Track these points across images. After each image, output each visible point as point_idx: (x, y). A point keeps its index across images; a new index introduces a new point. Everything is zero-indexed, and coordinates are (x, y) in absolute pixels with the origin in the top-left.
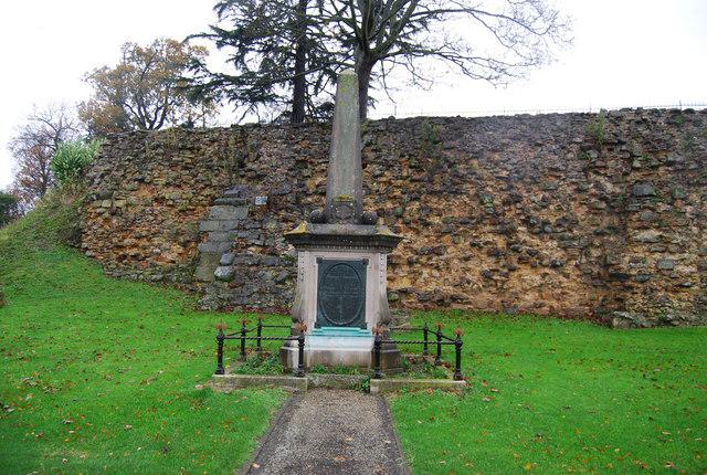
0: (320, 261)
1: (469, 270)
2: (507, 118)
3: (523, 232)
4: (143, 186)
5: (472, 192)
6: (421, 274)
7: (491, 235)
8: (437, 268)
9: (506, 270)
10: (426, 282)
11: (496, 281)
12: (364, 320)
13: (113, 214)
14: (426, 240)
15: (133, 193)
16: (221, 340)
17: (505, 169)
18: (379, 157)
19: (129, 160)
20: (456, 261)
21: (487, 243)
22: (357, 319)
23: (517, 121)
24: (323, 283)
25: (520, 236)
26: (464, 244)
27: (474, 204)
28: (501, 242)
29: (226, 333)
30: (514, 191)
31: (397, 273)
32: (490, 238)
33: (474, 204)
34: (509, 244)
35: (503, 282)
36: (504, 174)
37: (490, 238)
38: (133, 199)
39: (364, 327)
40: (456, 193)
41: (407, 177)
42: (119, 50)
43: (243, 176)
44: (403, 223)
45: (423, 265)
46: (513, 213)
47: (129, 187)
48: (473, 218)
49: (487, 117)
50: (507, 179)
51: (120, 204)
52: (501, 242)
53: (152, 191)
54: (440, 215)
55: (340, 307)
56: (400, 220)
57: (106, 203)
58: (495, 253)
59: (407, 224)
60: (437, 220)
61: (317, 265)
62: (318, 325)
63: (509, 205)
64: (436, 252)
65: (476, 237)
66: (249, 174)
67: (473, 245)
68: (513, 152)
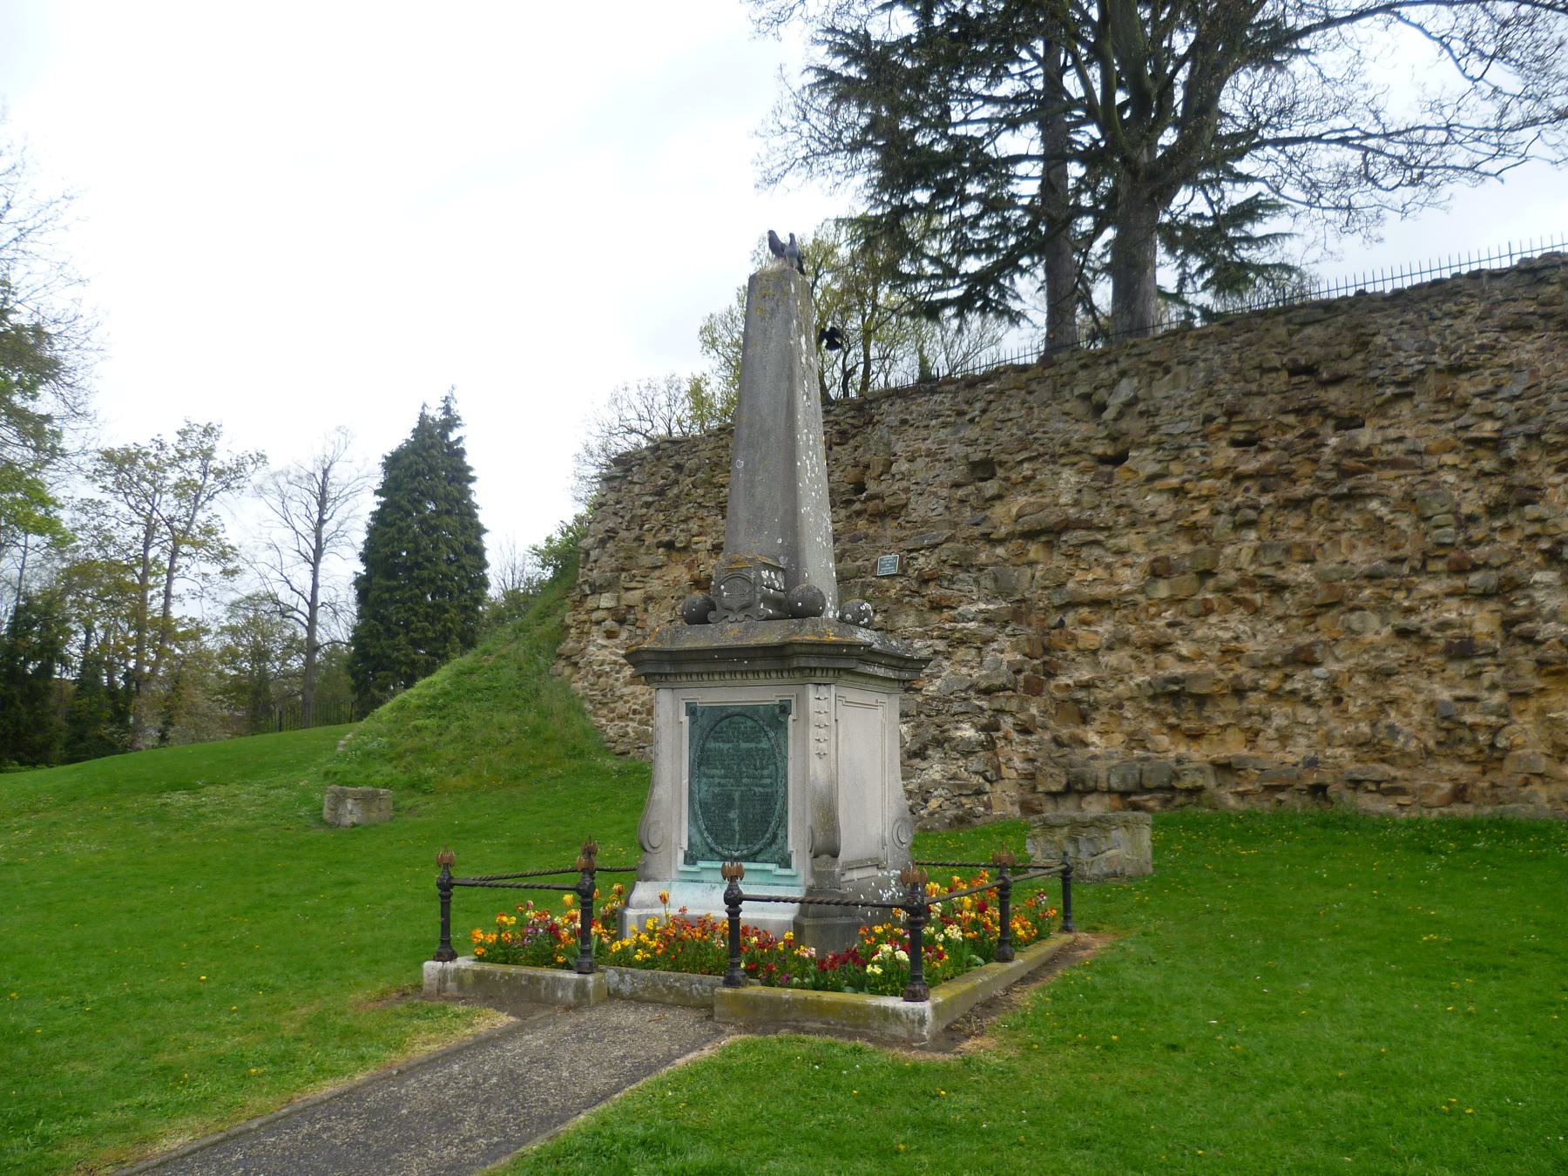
0: (692, 711)
1: (1393, 702)
2: (1495, 275)
3: (1548, 586)
4: (675, 555)
5: (1396, 490)
6: (1267, 718)
7: (1454, 603)
8: (1308, 701)
9: (1498, 698)
10: (1284, 738)
11: (1473, 728)
12: (784, 847)
13: (621, 622)
14: (1280, 628)
15: (657, 573)
16: (446, 887)
17: (1490, 415)
18: (1153, 429)
19: (648, 505)
20: (1360, 680)
21: (1443, 626)
22: (712, 850)
23: (1527, 278)
24: (701, 761)
25: (1539, 596)
26: (1375, 629)
27: (1404, 522)
28: (1483, 621)
29: (458, 874)
30: (1521, 476)
31: (1208, 719)
32: (1451, 611)
33: (1404, 522)
34: (1507, 624)
35: (1495, 731)
36: (1488, 428)
37: (1451, 611)
38: (655, 586)
39: (785, 863)
40: (1352, 498)
41: (1225, 471)
42: (1482, 187)
43: (859, 514)
44: (1216, 590)
45: (1274, 695)
46: (1518, 534)
47: (646, 561)
48: (1401, 561)
49: (1436, 283)
50: (1495, 444)
51: (635, 596)
52: (1483, 621)
53: (690, 567)
54: (1310, 560)
55: (733, 815)
56: (1211, 583)
57: (606, 601)
58: (1463, 650)
59: (1226, 590)
60: (1300, 573)
61: (685, 719)
62: (690, 859)
63: (1506, 512)
64: (1304, 658)
65: (1409, 611)
66: (871, 505)
67: (1402, 633)
68: (1510, 367)
